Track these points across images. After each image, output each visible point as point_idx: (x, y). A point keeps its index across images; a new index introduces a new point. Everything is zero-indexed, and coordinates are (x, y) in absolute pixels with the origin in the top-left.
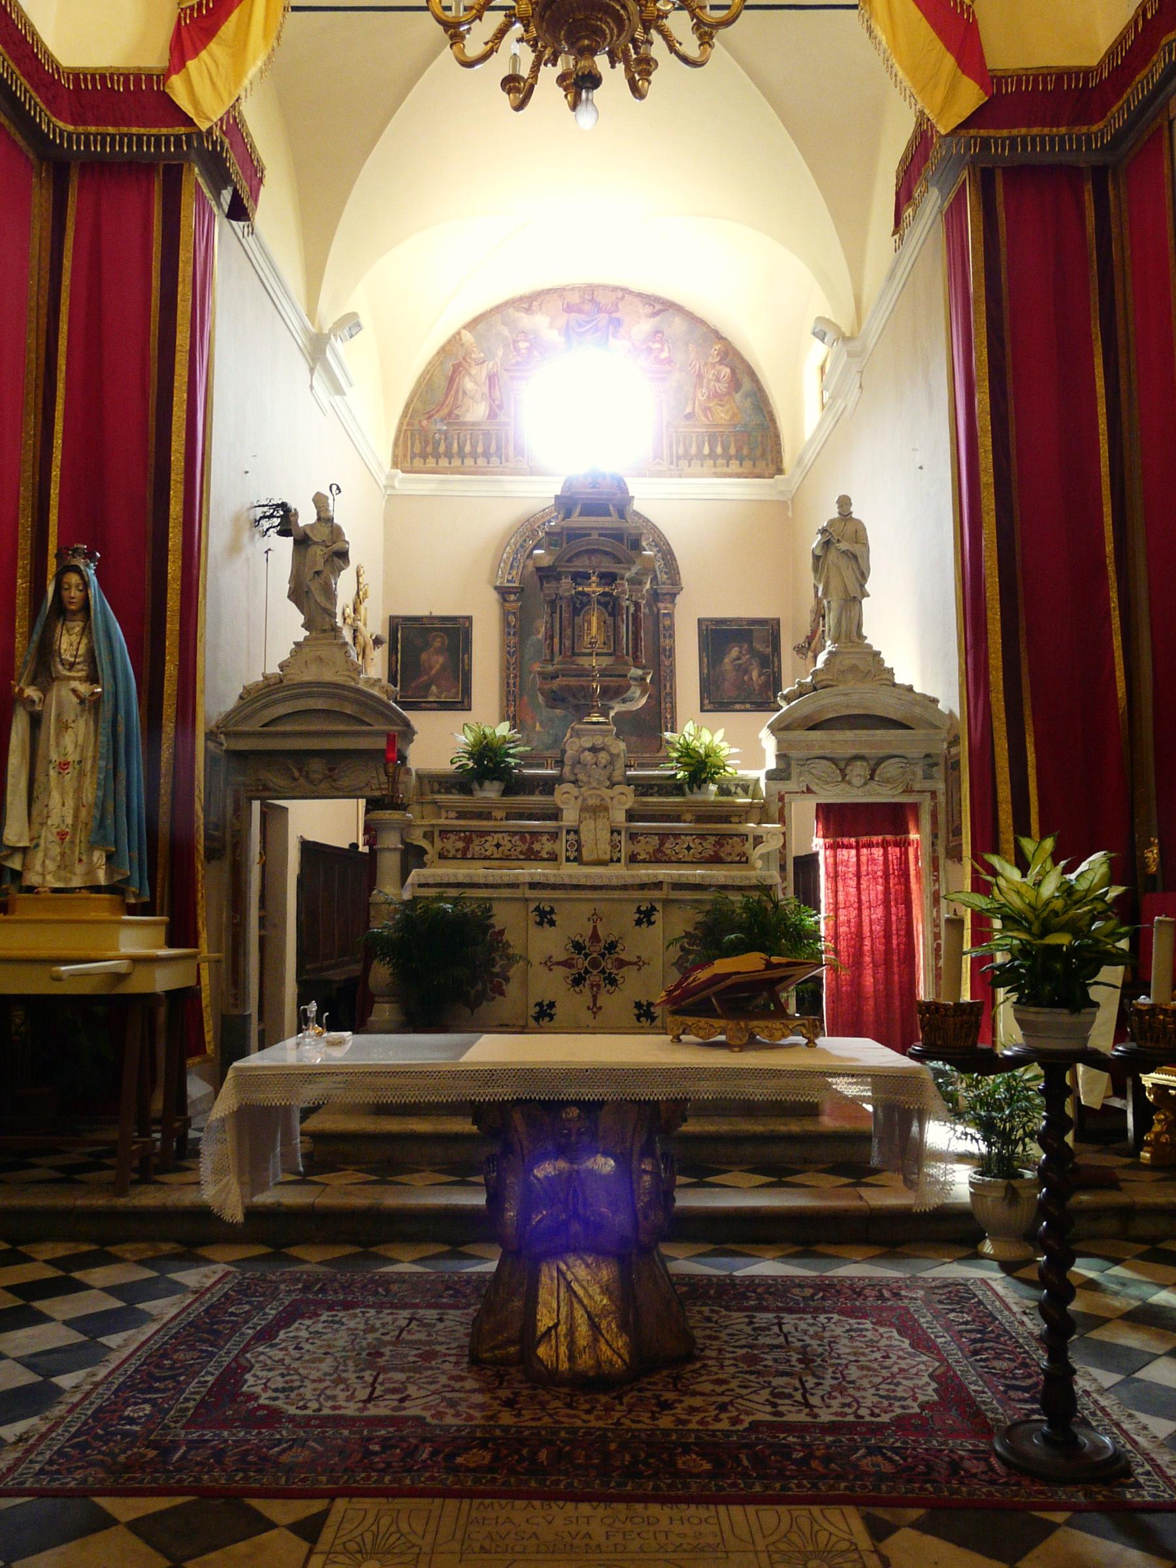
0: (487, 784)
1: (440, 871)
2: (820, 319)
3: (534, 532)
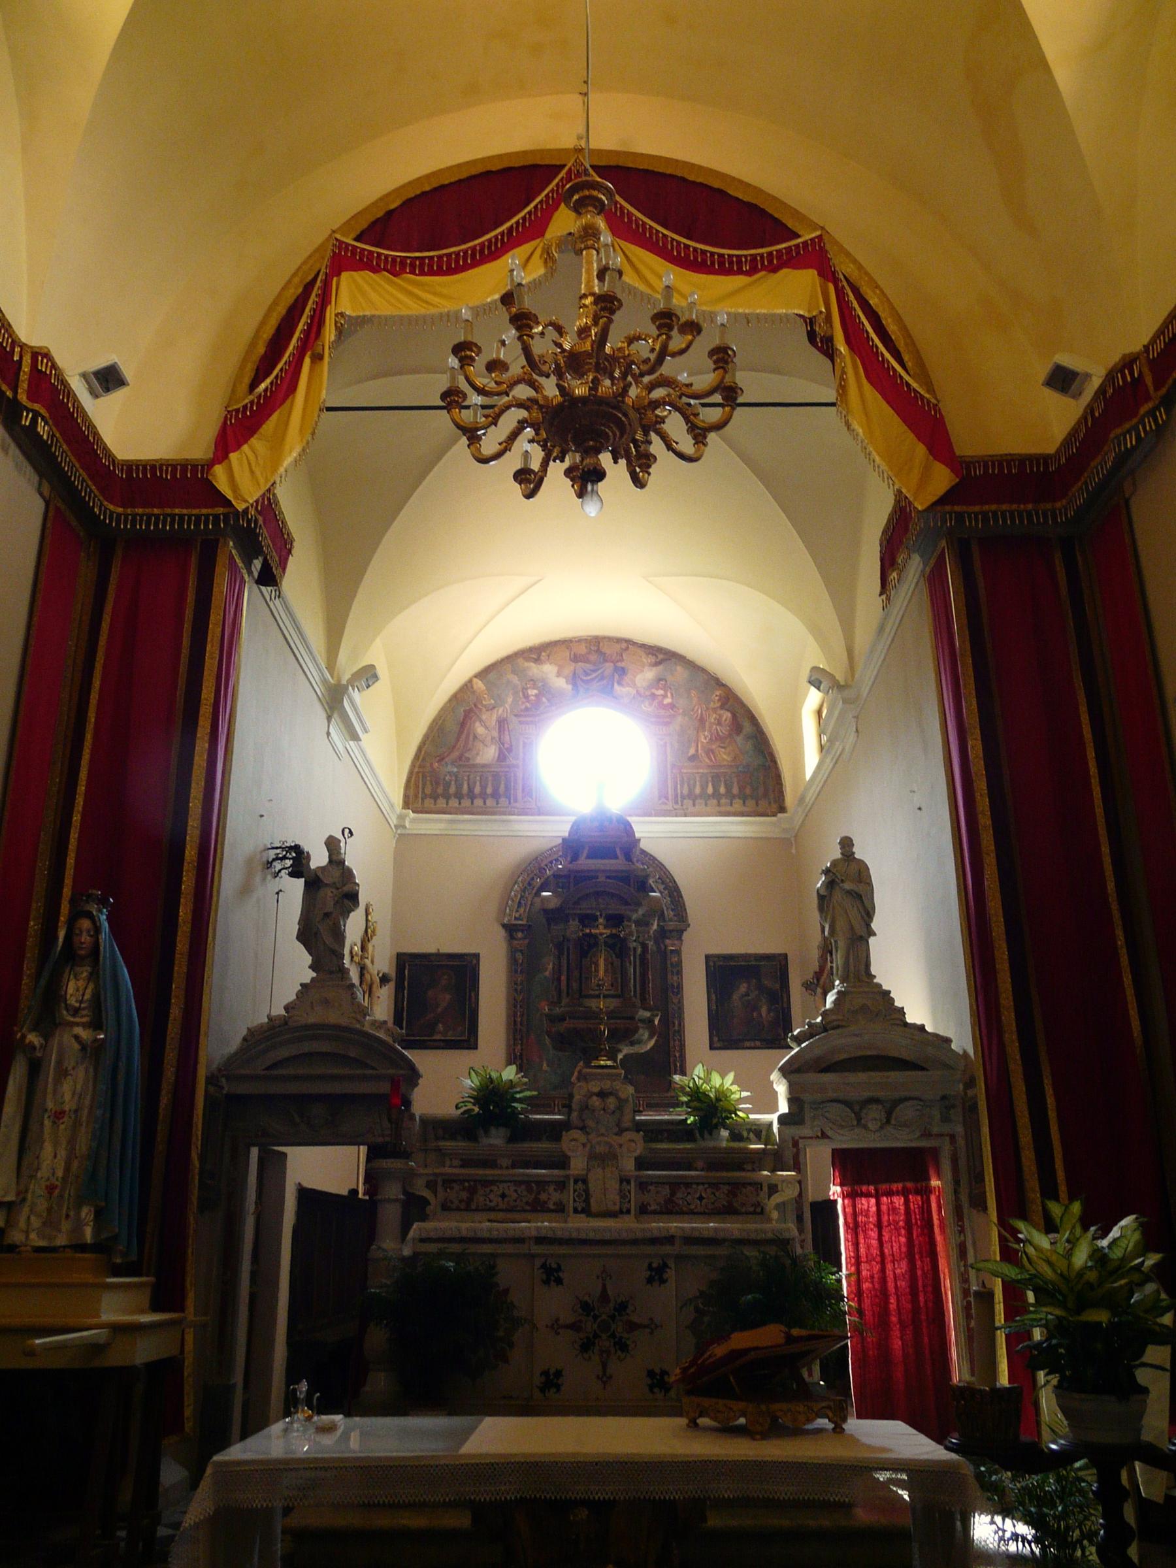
0: (493, 1131)
1: (445, 1225)
2: (815, 669)
3: (542, 870)
